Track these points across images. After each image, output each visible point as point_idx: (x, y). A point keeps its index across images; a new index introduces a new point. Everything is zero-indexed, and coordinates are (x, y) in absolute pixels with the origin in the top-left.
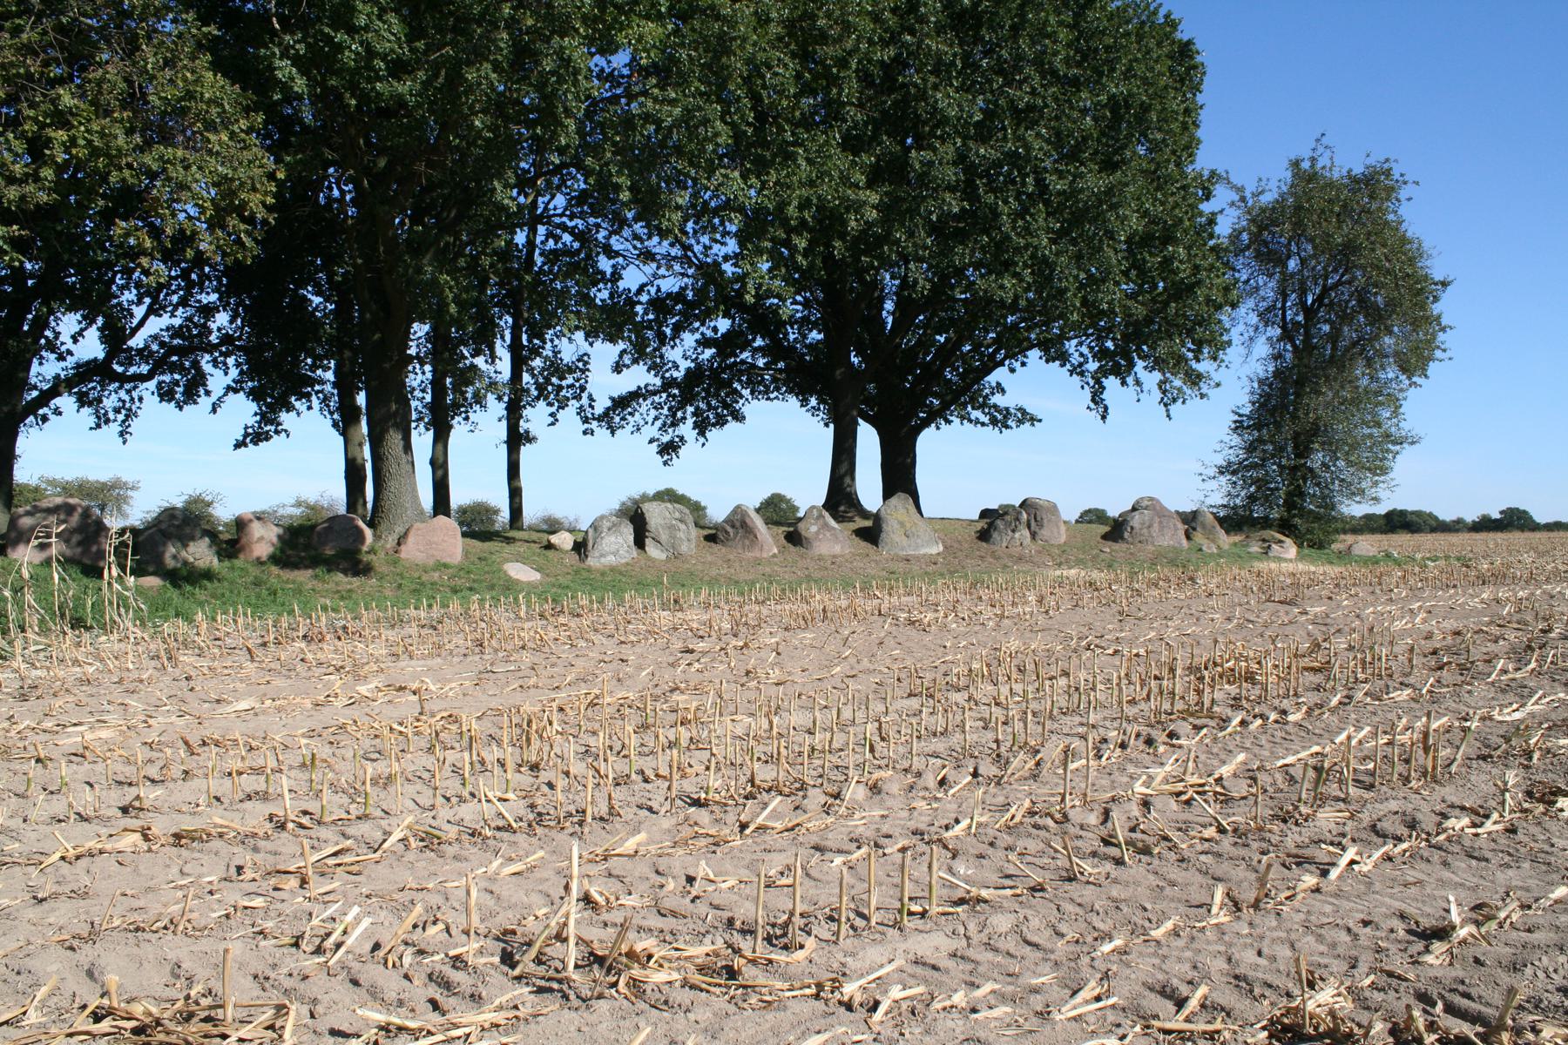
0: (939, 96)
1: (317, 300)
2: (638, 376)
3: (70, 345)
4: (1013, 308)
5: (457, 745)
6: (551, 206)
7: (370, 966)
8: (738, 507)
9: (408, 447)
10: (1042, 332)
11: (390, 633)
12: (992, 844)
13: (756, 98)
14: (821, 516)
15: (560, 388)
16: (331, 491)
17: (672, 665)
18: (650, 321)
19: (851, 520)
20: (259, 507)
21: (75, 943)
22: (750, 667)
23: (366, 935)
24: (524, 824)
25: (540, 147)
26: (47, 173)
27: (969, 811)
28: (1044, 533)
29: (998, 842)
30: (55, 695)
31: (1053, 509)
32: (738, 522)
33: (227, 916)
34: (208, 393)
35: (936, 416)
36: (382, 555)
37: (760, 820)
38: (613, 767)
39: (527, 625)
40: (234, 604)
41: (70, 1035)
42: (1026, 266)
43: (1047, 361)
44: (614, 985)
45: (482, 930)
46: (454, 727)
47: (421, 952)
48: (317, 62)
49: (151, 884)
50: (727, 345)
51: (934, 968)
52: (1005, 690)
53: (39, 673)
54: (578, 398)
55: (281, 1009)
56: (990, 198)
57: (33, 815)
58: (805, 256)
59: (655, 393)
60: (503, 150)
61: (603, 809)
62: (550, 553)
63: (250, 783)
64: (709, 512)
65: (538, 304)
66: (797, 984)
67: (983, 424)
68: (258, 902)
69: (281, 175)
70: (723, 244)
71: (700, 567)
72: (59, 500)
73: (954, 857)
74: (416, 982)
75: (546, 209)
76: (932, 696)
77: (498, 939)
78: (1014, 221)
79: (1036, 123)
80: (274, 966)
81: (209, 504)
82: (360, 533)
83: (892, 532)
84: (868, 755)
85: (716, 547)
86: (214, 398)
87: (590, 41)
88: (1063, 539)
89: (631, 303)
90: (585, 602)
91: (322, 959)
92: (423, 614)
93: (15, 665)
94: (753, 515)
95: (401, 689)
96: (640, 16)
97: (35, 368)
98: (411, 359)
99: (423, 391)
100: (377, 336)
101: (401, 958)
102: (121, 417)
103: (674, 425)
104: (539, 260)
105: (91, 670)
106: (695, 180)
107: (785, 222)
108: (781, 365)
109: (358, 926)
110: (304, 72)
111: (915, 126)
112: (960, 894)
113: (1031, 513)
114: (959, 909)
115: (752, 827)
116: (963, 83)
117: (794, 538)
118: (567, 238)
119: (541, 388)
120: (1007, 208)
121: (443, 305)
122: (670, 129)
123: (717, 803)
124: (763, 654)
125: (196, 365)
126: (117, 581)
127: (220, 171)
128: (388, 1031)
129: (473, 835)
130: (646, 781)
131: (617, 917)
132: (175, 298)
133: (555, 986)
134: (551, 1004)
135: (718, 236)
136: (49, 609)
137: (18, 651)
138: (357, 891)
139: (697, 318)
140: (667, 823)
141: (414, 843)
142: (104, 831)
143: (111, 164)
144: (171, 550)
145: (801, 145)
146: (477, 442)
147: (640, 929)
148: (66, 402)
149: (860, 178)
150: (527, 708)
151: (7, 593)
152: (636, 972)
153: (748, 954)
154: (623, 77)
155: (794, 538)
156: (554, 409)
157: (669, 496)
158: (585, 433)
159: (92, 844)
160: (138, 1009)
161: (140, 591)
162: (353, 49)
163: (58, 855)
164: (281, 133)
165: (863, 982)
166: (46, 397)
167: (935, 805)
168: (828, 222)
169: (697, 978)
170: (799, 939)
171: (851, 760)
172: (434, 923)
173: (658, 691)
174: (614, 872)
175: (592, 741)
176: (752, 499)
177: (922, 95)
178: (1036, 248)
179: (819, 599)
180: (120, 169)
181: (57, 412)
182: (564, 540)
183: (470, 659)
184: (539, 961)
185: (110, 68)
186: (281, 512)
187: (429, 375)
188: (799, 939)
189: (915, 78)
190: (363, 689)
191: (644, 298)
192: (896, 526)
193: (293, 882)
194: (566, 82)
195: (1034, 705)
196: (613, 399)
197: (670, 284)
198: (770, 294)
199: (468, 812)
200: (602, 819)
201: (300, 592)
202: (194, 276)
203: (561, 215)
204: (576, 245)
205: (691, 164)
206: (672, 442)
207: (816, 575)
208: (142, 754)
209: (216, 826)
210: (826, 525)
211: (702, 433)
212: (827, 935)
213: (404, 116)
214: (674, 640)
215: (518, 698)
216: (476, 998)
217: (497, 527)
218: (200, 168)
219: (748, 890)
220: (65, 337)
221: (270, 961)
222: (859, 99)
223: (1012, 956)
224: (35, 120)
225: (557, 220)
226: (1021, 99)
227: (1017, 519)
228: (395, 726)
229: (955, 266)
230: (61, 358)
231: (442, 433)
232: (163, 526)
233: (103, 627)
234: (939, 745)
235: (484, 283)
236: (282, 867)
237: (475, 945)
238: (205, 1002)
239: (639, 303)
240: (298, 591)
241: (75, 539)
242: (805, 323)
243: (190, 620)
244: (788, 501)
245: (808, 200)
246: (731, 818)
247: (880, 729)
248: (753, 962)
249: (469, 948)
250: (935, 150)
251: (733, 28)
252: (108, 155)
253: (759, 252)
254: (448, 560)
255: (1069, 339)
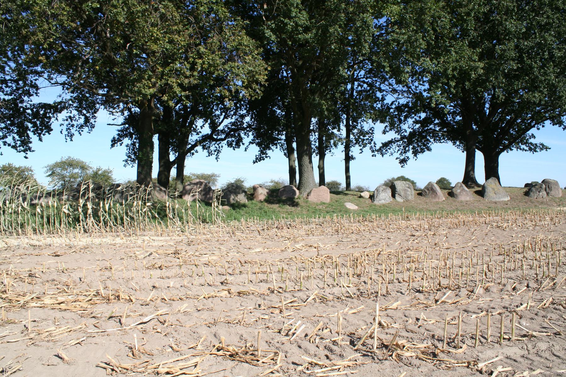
0: (507, 23)
1: (279, 111)
2: (392, 135)
3: (200, 130)
4: (539, 105)
5: (331, 267)
6: (359, 75)
7: (304, 342)
8: (430, 183)
9: (311, 162)
10: (551, 113)
11: (305, 226)
12: (536, 314)
13: (434, 30)
14: (461, 186)
15: (364, 140)
16: (285, 178)
17: (407, 240)
18: (396, 115)
19: (473, 187)
20: (260, 182)
21: (210, 325)
22: (436, 242)
23: (303, 331)
24: (356, 296)
25: (354, 53)
26: (196, 73)
27: (528, 301)
28: (552, 193)
29: (539, 314)
30: (198, 244)
31: (556, 183)
32: (430, 188)
33: (257, 321)
34: (243, 144)
35: (507, 147)
36: (302, 199)
37: (443, 299)
38: (388, 277)
39: (354, 225)
40: (253, 216)
41: (211, 354)
42: (545, 88)
43: (553, 125)
44: (391, 355)
45: (343, 332)
46: (330, 260)
47: (322, 338)
48: (279, 30)
49: (231, 308)
50: (424, 123)
51: (515, 360)
52: (538, 254)
53: (193, 237)
54: (370, 143)
55: (276, 353)
56: (529, 62)
57: (195, 283)
58: (454, 89)
59: (398, 141)
60: (341, 57)
61: (384, 292)
62: (361, 199)
63: (262, 277)
64: (417, 184)
65: (356, 109)
66: (460, 362)
67: (526, 150)
68: (266, 317)
69: (269, 69)
70: (423, 85)
71: (416, 205)
72: (198, 180)
73: (521, 318)
74: (321, 348)
75: (357, 76)
76: (508, 255)
77: (348, 336)
78: (540, 70)
79: (549, 30)
80: (273, 339)
81: (243, 182)
82: (294, 191)
83: (489, 192)
84: (484, 277)
85: (421, 198)
86: (245, 146)
87: (373, 14)
88: (560, 195)
89: (389, 109)
90: (374, 217)
91: (288, 338)
92: (317, 220)
93: (186, 234)
94: (436, 186)
95: (311, 246)
96: (391, 4)
97: (190, 137)
98: (311, 131)
99: (315, 142)
100: (300, 123)
101: (315, 340)
102: (216, 153)
103: (405, 152)
104: (355, 94)
105: (209, 236)
106: (412, 62)
107: (447, 76)
108: (445, 130)
109: (301, 328)
110: (275, 34)
111: (498, 36)
112: (524, 333)
113: (547, 185)
114: (524, 339)
115: (440, 301)
116: (518, 17)
117: (451, 194)
118: (365, 86)
119: (357, 140)
120: (536, 65)
121: (322, 112)
122: (403, 44)
123: (427, 292)
124: (441, 237)
125: (239, 135)
126: (217, 208)
127: (248, 70)
128: (312, 365)
129: (338, 298)
130: (399, 282)
131: (393, 331)
132: (232, 113)
133: (370, 354)
134: (368, 361)
135: (421, 83)
136: (196, 218)
137: (187, 229)
138: (299, 316)
139: (413, 113)
140: (408, 298)
141: (318, 300)
142: (216, 290)
143: (215, 69)
144: (232, 197)
145: (452, 47)
146: (334, 159)
147: (400, 336)
148: (199, 148)
149: (476, 58)
150: (357, 254)
151: (183, 211)
152: (399, 351)
153: (441, 348)
154: (384, 26)
155: (451, 194)
156: (361, 147)
157: (402, 178)
158: (373, 156)
159: (213, 294)
160: (231, 348)
161: (223, 211)
162: (291, 24)
163: (203, 296)
164: (267, 56)
165: (486, 363)
166: (193, 147)
167: (512, 298)
168: (463, 75)
169: (421, 356)
170: (460, 345)
171: (477, 278)
172: (326, 329)
173: (402, 250)
174: (389, 315)
175: (379, 267)
176: (434, 180)
177: (501, 24)
178: (549, 80)
179: (462, 217)
180: (218, 71)
181: (197, 152)
182: (366, 195)
183: (334, 236)
184: (363, 345)
185: (215, 39)
186: (266, 184)
187: (317, 136)
188: (460, 345)
189: (498, 17)
190: (298, 246)
191: (394, 106)
192: (491, 190)
193: (277, 311)
194: (365, 30)
195: (551, 261)
196: (382, 144)
197: (403, 101)
198: (441, 103)
199: (336, 290)
200: (384, 295)
201: (275, 212)
202: (238, 105)
203: (363, 78)
204: (368, 88)
205: (411, 56)
206: (404, 159)
207: (460, 208)
208: (227, 265)
209: (251, 290)
210: (463, 189)
211: (415, 155)
212: (470, 344)
213: (308, 46)
214: (407, 231)
215: (352, 251)
216: (341, 356)
217: (340, 190)
218: (243, 69)
219: (439, 325)
220: (199, 127)
221: (271, 337)
222: (475, 28)
223: (548, 360)
224: (193, 57)
225: (362, 80)
226: (543, 21)
227: (541, 187)
228: (309, 259)
229: (514, 90)
230: (198, 134)
231: (322, 157)
232: (230, 189)
233: (212, 223)
234: (512, 274)
235: (336, 103)
236: (273, 306)
237: (341, 337)
238: (252, 349)
239: (392, 108)
240: (274, 212)
241: (203, 193)
242: (454, 114)
243: (239, 221)
244: (447, 180)
245: (456, 67)
246: (432, 297)
247: (488, 267)
248: (443, 351)
249: (338, 338)
250: (505, 44)
251: (426, 5)
252: (214, 67)
253: (437, 88)
254: (325, 201)
255: (563, 116)
